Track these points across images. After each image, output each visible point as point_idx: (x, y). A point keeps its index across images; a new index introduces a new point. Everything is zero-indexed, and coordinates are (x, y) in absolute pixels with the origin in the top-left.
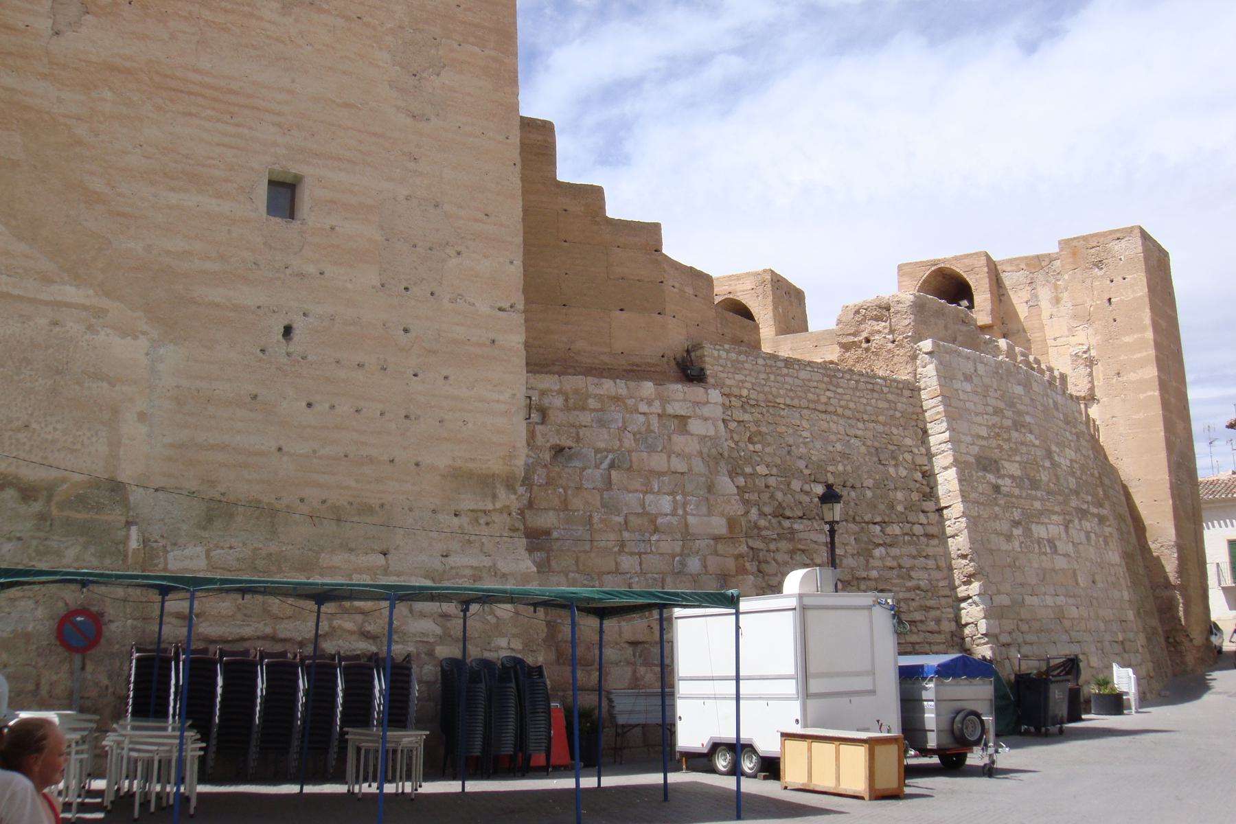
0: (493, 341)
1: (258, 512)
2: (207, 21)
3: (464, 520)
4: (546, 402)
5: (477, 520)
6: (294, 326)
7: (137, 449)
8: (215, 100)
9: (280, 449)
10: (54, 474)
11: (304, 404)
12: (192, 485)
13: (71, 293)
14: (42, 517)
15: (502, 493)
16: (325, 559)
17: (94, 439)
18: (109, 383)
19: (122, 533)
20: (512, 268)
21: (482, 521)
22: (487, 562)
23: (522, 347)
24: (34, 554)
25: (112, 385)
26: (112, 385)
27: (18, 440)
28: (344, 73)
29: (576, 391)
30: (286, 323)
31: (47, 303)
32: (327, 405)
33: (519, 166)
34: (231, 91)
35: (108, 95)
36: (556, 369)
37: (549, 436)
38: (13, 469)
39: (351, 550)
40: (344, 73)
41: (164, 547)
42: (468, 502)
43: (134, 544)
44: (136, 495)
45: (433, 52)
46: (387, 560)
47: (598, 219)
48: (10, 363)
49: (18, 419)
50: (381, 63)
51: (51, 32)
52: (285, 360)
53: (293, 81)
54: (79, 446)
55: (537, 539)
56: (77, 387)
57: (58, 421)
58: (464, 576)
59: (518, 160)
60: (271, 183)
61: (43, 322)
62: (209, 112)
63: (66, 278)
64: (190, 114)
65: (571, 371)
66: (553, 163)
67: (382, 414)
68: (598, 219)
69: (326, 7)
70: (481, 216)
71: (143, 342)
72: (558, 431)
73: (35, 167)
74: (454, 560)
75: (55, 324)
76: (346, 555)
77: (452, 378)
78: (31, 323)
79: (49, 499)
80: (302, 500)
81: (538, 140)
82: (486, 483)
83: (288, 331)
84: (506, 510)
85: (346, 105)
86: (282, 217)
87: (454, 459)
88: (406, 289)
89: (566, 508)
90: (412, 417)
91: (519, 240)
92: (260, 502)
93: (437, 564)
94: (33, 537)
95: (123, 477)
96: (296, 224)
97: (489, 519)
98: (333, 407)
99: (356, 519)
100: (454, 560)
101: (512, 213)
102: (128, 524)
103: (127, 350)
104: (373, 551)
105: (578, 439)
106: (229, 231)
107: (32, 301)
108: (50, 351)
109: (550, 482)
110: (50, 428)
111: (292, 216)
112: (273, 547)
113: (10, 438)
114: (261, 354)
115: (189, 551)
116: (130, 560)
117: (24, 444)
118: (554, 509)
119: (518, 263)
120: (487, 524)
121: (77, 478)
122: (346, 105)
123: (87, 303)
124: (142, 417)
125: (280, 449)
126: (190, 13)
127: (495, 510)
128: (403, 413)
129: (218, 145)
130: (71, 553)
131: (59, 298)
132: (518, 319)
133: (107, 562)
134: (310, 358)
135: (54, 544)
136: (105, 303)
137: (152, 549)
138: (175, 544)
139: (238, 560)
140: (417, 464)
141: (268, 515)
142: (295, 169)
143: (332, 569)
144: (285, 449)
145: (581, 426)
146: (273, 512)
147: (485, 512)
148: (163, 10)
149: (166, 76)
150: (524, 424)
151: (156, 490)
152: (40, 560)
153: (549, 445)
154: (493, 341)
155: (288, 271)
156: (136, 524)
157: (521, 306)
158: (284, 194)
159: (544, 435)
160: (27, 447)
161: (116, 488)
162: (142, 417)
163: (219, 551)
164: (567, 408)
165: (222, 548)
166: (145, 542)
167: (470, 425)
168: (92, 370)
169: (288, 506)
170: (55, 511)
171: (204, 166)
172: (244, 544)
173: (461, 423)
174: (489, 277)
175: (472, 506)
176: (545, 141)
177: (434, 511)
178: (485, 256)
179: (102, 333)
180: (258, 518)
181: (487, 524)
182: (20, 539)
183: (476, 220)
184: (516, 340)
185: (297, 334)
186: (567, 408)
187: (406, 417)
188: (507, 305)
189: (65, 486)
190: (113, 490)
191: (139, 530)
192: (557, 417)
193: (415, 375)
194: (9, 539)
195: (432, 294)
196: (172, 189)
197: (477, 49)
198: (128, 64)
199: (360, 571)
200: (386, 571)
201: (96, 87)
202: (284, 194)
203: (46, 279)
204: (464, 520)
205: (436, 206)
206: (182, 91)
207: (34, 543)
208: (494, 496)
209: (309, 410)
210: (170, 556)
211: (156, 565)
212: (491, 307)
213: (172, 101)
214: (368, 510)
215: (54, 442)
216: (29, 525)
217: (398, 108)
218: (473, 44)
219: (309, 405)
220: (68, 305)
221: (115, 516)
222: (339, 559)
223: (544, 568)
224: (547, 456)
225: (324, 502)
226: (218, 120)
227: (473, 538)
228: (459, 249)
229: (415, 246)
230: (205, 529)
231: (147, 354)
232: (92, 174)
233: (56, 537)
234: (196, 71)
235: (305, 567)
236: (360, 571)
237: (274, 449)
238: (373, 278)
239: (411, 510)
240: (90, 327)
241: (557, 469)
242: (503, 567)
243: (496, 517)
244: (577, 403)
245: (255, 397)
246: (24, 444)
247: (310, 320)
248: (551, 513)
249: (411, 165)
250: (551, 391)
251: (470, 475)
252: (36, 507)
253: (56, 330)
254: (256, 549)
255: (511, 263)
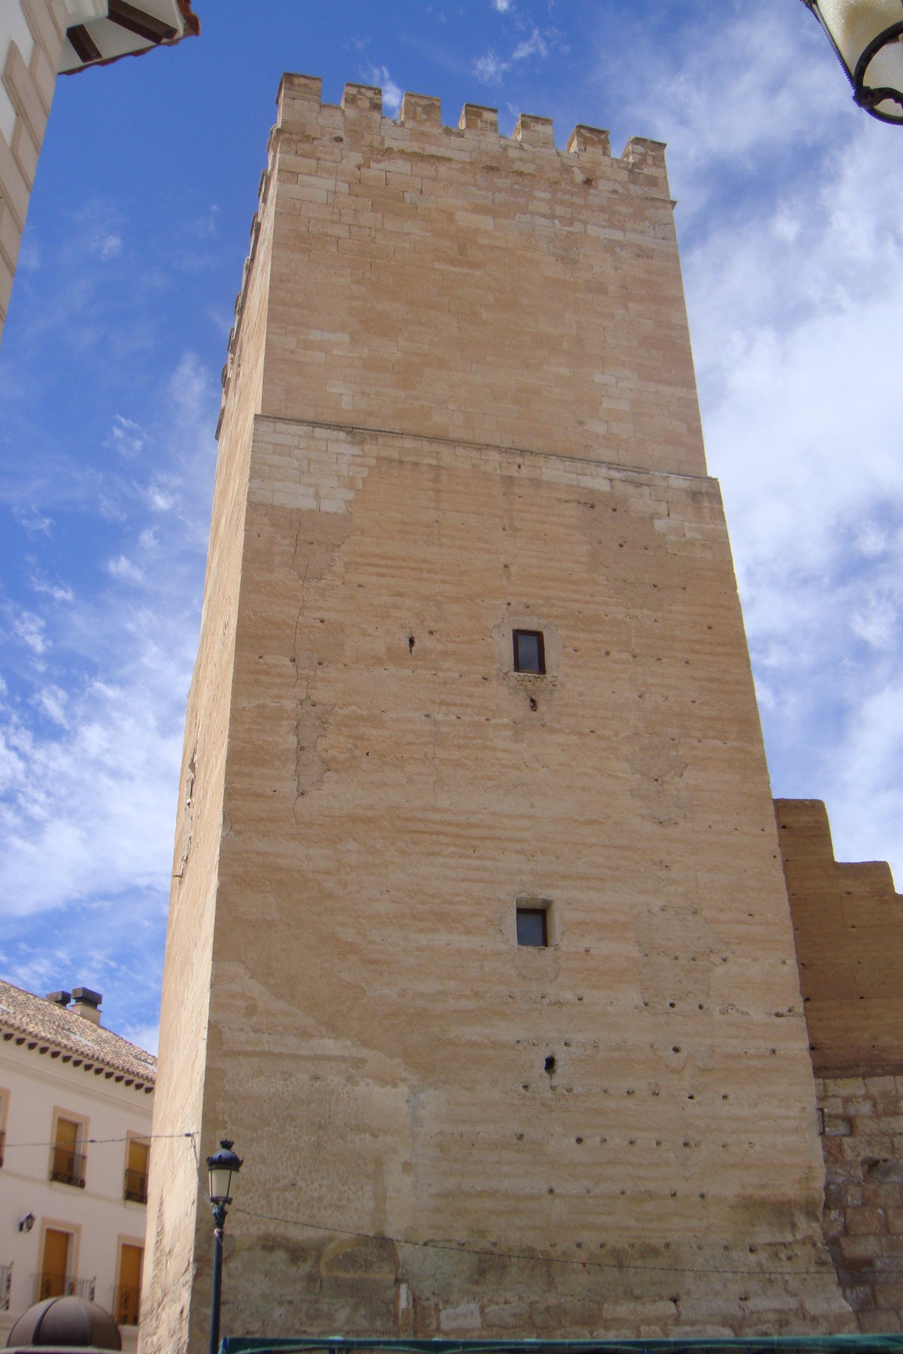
0: (774, 1051)
1: (532, 1261)
2: (442, 760)
3: (762, 1256)
4: (851, 1110)
5: (776, 1255)
6: (557, 1057)
7: (404, 1203)
8: (457, 836)
9: (551, 1191)
10: (321, 1233)
11: (573, 1140)
12: (461, 1235)
13: (330, 1046)
14: (312, 1279)
15: (802, 1221)
16: (609, 1310)
17: (360, 1193)
18: (372, 1134)
19: (390, 1293)
20: (785, 969)
21: (783, 1256)
22: (793, 1303)
23: (806, 1054)
24: (304, 1319)
25: (375, 1135)
26: (375, 1135)
27: (285, 1199)
28: (583, 789)
29: (885, 1094)
30: (548, 1055)
31: (307, 1058)
32: (598, 1139)
33: (779, 858)
34: (471, 826)
35: (353, 845)
36: (861, 1070)
37: (856, 1150)
38: (281, 1230)
39: (637, 1298)
40: (583, 789)
41: (436, 1305)
42: (764, 1235)
43: (403, 1304)
44: (404, 1252)
45: (673, 753)
46: (677, 1307)
47: (886, 897)
48: (275, 1121)
49: (285, 1177)
50: (620, 774)
51: (296, 794)
52: (549, 1094)
53: (532, 806)
54: (345, 1202)
55: (853, 1272)
56: (340, 1141)
57: (323, 1178)
58: (768, 1322)
59: (778, 851)
60: (520, 911)
61: (305, 1077)
62: (452, 849)
63: (324, 1032)
64: (433, 854)
65: (878, 1071)
66: (829, 844)
67: (658, 1144)
68: (886, 897)
69: (558, 726)
70: (745, 917)
71: (403, 1089)
72: (868, 1141)
73: (289, 925)
74: (754, 1304)
75: (316, 1078)
76: (632, 1305)
77: (732, 1097)
78: (293, 1079)
79: (318, 1258)
80: (579, 1245)
81: (802, 825)
82: (781, 1211)
83: (550, 1064)
84: (809, 1240)
85: (589, 822)
86: (535, 945)
87: (743, 1186)
88: (672, 1005)
89: (888, 1231)
90: (692, 1144)
91: (790, 936)
92: (534, 1250)
93: (734, 1308)
94: (303, 1300)
95: (390, 1233)
96: (549, 950)
97: (790, 1253)
98: (604, 1141)
99: (639, 1262)
100: (754, 1304)
101: (778, 908)
102: (398, 1281)
103: (389, 1099)
104: (661, 1298)
105: (893, 1149)
106: (482, 967)
107: (292, 1057)
108: (312, 1106)
109: (866, 1202)
110: (316, 1185)
111: (545, 942)
112: (552, 1300)
113: (278, 1198)
114: (523, 1091)
115: (463, 1308)
116: (401, 1321)
117: (292, 1203)
118: (875, 1234)
119: (792, 962)
120: (789, 1258)
121: (346, 1236)
122: (589, 822)
123: (346, 1053)
124: (407, 1167)
125: (551, 1191)
126: (425, 754)
127: (796, 1242)
128: (681, 1141)
129: (463, 880)
130: (342, 1316)
131: (319, 1052)
132: (800, 1023)
133: (378, 1323)
134: (575, 1090)
135: (324, 1307)
136: (363, 1052)
137: (424, 1307)
138: (447, 1302)
139: (514, 1315)
140: (702, 1196)
141: (543, 1264)
142: (543, 894)
143: (617, 1322)
144: (557, 1190)
145: (895, 1134)
146: (548, 1261)
147: (784, 1245)
148: (399, 756)
149: (407, 819)
150: (819, 1140)
151: (425, 1244)
152: (311, 1325)
153: (860, 1159)
154: (774, 1051)
155: (546, 1001)
156: (406, 1281)
157: (800, 1009)
158: (535, 921)
159: (853, 1149)
160: (294, 1206)
161: (384, 1243)
162: (407, 1167)
163: (494, 1307)
164: (877, 1115)
165: (497, 1303)
166: (415, 1300)
167: (757, 1147)
168: (354, 1122)
169: (564, 1253)
170: (324, 1272)
171: (451, 903)
172: (521, 1298)
173: (747, 1146)
174: (761, 981)
175: (769, 1238)
176: (817, 821)
177: (726, 1248)
178: (754, 960)
179: (363, 1084)
180: (533, 1269)
181: (789, 1258)
182: (291, 1302)
183: (740, 922)
184: (798, 1046)
185: (560, 1067)
186: (877, 1115)
187: (686, 1144)
188: (783, 1010)
189: (333, 1245)
190: (381, 1246)
191: (409, 1287)
192: (866, 1126)
193: (691, 1097)
194: (281, 1304)
195: (700, 1007)
196: (422, 931)
197: (719, 743)
198: (369, 814)
199: (648, 1322)
200: (677, 1320)
201: (341, 840)
202: (535, 921)
203: (306, 1034)
204: (762, 1256)
205: (695, 913)
206: (423, 832)
207: (305, 1306)
208: (793, 1226)
209: (579, 1146)
210: (443, 1314)
211: (429, 1326)
212: (768, 1014)
213: (414, 843)
214: (651, 1252)
215: (320, 1199)
216: (299, 1288)
217: (643, 817)
218: (714, 738)
219: (579, 1140)
220: (328, 1058)
221: (384, 1274)
222: (623, 1310)
223: (864, 1309)
224: (860, 1172)
225: (602, 1246)
226: (462, 856)
227: (773, 1276)
228: (725, 955)
229: (676, 958)
230: (477, 1283)
231: (408, 1101)
232: (343, 924)
233: (326, 1300)
234: (435, 810)
235: (589, 1320)
236: (648, 1322)
237: (545, 1191)
238: (636, 999)
239: (700, 1248)
240: (350, 1079)
241: (872, 1187)
242: (813, 1307)
243: (798, 1250)
244: (888, 1107)
245: (521, 1137)
246: (292, 1203)
247: (573, 1049)
248: (872, 1239)
249: (663, 874)
250: (855, 1096)
251: (763, 1204)
252: (305, 1268)
253: (318, 1083)
254: (533, 1303)
255: (784, 963)
